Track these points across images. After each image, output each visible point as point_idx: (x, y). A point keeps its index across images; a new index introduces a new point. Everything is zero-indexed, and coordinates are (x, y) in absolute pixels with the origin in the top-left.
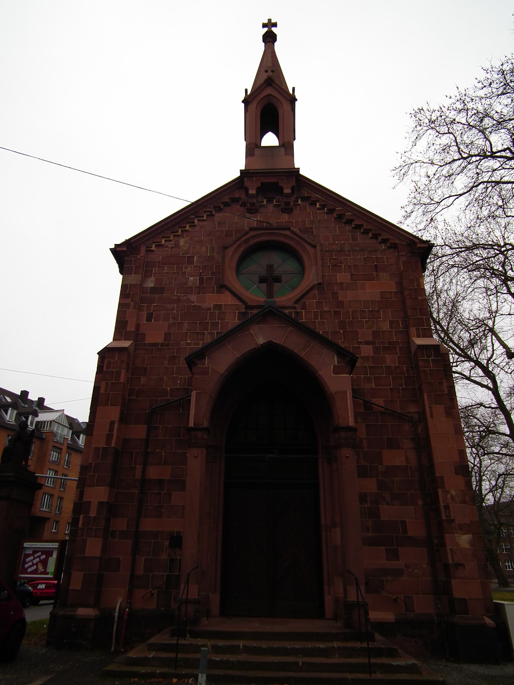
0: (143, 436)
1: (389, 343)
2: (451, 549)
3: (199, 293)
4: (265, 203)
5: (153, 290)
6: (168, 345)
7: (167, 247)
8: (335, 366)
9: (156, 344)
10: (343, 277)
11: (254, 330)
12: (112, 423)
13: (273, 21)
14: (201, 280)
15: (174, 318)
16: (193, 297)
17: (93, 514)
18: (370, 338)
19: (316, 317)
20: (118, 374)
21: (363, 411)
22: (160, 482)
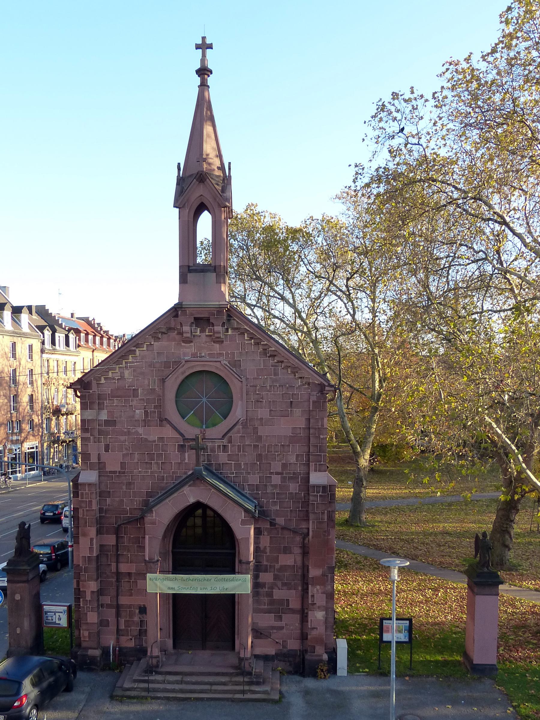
0: (114, 543)
1: (294, 473)
2: (311, 620)
3: (145, 426)
4: (198, 333)
5: (107, 423)
6: (124, 473)
7: (114, 379)
8: (242, 520)
9: (115, 472)
10: (263, 413)
11: (186, 490)
12: (92, 540)
13: (208, 42)
14: (146, 413)
15: (126, 449)
16: (140, 430)
17: (88, 598)
18: (280, 470)
19: (239, 451)
20: (91, 502)
21: (269, 527)
22: (129, 574)
